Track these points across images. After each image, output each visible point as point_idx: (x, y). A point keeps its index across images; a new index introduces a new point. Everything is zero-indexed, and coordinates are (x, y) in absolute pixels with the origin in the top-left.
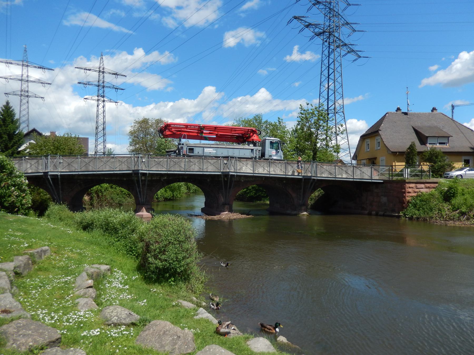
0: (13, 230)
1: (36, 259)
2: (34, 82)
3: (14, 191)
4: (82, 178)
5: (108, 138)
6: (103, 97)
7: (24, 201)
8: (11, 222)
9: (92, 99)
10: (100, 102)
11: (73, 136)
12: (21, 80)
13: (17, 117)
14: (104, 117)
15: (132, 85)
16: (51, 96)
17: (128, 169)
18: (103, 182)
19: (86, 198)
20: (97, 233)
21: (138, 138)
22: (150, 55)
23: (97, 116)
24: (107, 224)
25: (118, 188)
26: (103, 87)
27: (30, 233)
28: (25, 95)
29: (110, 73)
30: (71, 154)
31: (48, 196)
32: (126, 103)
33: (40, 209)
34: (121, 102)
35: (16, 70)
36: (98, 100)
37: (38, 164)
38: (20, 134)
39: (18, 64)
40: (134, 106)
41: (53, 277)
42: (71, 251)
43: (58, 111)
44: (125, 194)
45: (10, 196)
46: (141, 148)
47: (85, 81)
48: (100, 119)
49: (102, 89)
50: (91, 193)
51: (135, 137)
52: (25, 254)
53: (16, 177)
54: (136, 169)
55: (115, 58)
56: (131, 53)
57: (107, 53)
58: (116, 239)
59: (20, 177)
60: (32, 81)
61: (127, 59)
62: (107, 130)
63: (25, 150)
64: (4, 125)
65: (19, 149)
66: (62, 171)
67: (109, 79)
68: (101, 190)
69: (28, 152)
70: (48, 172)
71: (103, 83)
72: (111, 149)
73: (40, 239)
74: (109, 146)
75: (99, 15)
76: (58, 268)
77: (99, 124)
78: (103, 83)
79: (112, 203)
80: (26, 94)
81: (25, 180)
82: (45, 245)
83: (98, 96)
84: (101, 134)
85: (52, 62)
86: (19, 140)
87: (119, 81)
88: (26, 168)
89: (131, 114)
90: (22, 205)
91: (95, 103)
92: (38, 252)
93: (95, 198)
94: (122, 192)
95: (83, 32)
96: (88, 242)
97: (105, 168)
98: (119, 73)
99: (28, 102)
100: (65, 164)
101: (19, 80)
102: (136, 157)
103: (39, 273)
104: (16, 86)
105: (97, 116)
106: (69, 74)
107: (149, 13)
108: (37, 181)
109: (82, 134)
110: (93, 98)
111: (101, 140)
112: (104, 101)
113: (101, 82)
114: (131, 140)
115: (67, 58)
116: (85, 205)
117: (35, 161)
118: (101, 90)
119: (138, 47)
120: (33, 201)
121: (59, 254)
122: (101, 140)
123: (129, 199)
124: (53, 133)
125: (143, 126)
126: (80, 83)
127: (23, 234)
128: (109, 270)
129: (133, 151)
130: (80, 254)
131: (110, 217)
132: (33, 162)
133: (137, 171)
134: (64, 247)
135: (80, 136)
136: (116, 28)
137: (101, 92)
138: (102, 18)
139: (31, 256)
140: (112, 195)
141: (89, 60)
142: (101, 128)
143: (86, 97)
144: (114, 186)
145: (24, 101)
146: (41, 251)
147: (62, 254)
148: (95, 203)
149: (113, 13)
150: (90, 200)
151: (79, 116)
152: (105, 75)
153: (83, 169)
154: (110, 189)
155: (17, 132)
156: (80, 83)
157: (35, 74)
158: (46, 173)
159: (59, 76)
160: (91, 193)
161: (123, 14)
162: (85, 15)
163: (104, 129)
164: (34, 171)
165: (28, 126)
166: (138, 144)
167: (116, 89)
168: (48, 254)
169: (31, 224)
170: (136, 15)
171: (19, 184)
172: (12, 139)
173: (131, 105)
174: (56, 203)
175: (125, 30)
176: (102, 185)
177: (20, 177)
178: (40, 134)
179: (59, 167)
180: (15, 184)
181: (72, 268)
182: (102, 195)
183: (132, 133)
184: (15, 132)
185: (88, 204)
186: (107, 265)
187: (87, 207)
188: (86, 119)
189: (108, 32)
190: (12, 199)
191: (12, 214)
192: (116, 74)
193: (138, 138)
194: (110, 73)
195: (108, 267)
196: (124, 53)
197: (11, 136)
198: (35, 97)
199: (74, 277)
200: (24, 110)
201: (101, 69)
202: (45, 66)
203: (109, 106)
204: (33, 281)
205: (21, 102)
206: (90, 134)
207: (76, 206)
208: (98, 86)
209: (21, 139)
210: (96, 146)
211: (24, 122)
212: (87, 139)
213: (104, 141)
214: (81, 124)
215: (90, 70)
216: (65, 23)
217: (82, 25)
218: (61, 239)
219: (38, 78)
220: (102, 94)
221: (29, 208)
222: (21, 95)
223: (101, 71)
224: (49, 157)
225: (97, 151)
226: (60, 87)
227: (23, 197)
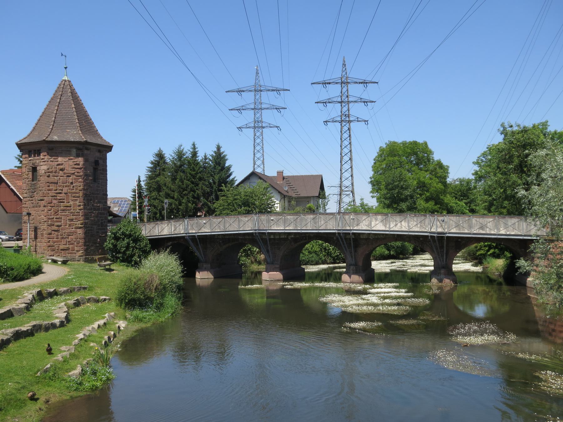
49: (347, 106)
167: (364, 102)
220: (347, 113)
222: (255, 127)
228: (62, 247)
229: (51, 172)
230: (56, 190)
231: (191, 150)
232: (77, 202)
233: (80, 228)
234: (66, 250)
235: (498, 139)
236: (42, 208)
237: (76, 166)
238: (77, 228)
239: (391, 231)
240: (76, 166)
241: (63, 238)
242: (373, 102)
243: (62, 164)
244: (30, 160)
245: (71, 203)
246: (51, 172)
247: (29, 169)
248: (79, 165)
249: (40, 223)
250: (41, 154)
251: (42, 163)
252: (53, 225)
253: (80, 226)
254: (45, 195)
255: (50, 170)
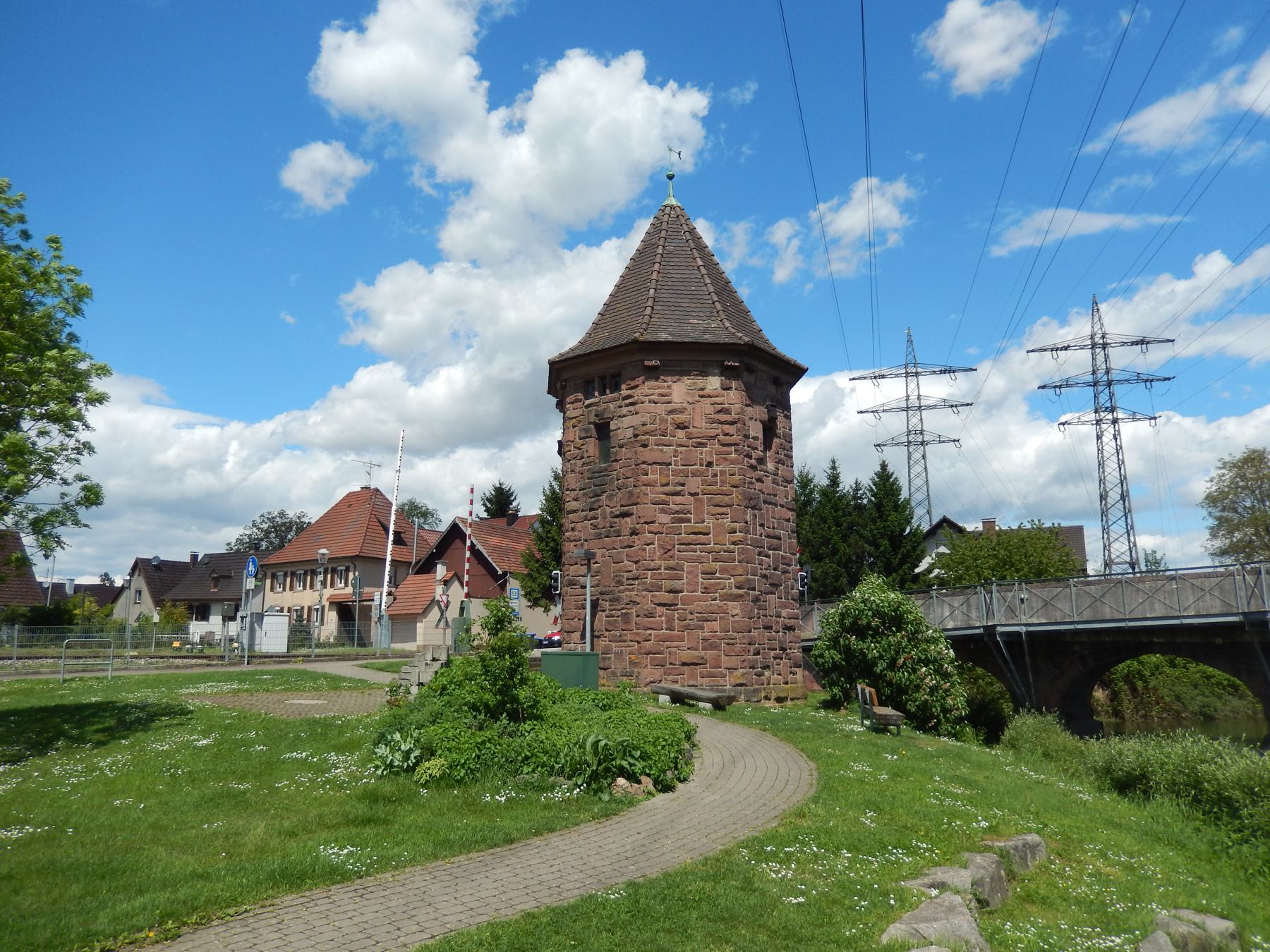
0: (943, 777)
1: (1015, 868)
2: (934, 407)
3: (926, 676)
4: (1085, 639)
5: (1138, 519)
6: (1112, 410)
7: (950, 701)
8: (933, 756)
9: (1080, 422)
10: (1104, 426)
11: (1048, 524)
12: (907, 409)
13: (904, 494)
14: (1121, 464)
15: (1198, 362)
16: (976, 434)
17: (1224, 610)
18: (1150, 650)
19: (1099, 694)
20: (1165, 809)
21: (1235, 511)
22: (1247, 262)
23: (1101, 465)
24: (1197, 784)
25: (1193, 667)
26: (1109, 384)
27: (984, 790)
28: (916, 440)
29: (1124, 344)
30: (1039, 575)
31: (998, 686)
32: (1184, 415)
33: (988, 724)
34: (1166, 413)
35: (894, 389)
36: (1098, 422)
37: (969, 606)
38: (914, 533)
39: (897, 376)
40: (1213, 417)
41: (1071, 927)
42: (1103, 854)
43: (996, 465)
44: (1218, 684)
45: (918, 688)
46: (1251, 541)
47: (1057, 379)
48: (1108, 470)
49: (1107, 391)
50: (1111, 681)
51: (1223, 510)
52: (988, 849)
53: (928, 641)
54: (1253, 609)
55: (1137, 298)
56: (1185, 272)
57: (1112, 294)
58: (1234, 836)
59: (935, 641)
60: (928, 407)
61: (1173, 291)
62: (1135, 499)
63: (929, 570)
64: (880, 517)
65: (917, 571)
66: (1030, 621)
67: (1122, 359)
68: (1139, 672)
69: (936, 577)
70: (995, 626)
71: (1107, 373)
72: (1155, 552)
73: (1013, 811)
74: (1145, 542)
75: (1081, 205)
76: (1078, 902)
77: (1109, 486)
78: (1107, 373)
79: (1178, 713)
80: (920, 438)
81: (947, 648)
82: (1030, 831)
83: (1096, 411)
84: (1116, 513)
85: (973, 351)
86: (914, 549)
87: (1155, 359)
88: (945, 616)
89: (1201, 443)
90: (945, 711)
91: (1091, 430)
92: (1016, 848)
93: (1126, 695)
94: (1209, 678)
95: (1042, 261)
96: (1146, 834)
97: (1152, 609)
98: (1150, 336)
99: (924, 457)
100: (1037, 604)
101: (902, 409)
102: (1251, 572)
103: (1033, 909)
104: (896, 424)
105: (1101, 465)
106: (1013, 371)
107: (1229, 150)
108: (975, 648)
109: (1062, 518)
110: (1083, 419)
111: (1118, 529)
112: (1115, 421)
113: (1101, 373)
114: (1211, 522)
115: (1005, 332)
116: (1098, 714)
117: (961, 598)
118: (1104, 391)
119: (1207, 251)
120: (970, 702)
121: (1069, 860)
122: (1118, 529)
123: (1235, 702)
124: (989, 524)
125: (1250, 472)
126: (1043, 387)
127: (968, 792)
128: (1233, 936)
129: (1223, 553)
130: (1129, 868)
131: (1202, 762)
132: (957, 601)
133: (1260, 617)
134: (1081, 841)
135: (1064, 524)
136: (1129, 222)
137: (1104, 398)
138: (1091, 209)
139: (1001, 856)
140: (1178, 688)
141: (1064, 322)
142: (1114, 495)
143: (1063, 419)
144: (1179, 660)
145: (917, 455)
146: (1024, 846)
147: (1079, 862)
148: (1127, 707)
149: (1121, 188)
150: (1112, 700)
151: (1051, 470)
152: (1110, 350)
153: (1087, 615)
154: (1168, 670)
155: (908, 530)
156: (1043, 387)
157: (935, 388)
158: (990, 630)
159: (991, 379)
160: (1111, 681)
161: (1149, 181)
162: (1044, 217)
163: (1124, 497)
164: (959, 624)
165: (929, 512)
166: (1238, 528)
167: (1146, 381)
168: (1041, 857)
169: (980, 766)
170: (1188, 169)
171: (935, 660)
172: (899, 547)
173: (1203, 417)
174: (1029, 711)
175: (1157, 220)
176: (1144, 658)
177: (935, 641)
178: (961, 530)
179: (1022, 611)
180: (927, 658)
181: (1117, 910)
182: (1146, 688)
183: (1211, 500)
184: (904, 530)
185: (1107, 712)
186: (1223, 917)
187: (1103, 719)
188: (1068, 475)
189: (1112, 235)
190: (923, 696)
191: (925, 732)
192: (1142, 342)
193: (1235, 511)
194: (1124, 344)
195: (1229, 925)
196: (1165, 277)
197: (897, 539)
198: (940, 442)
199: (1130, 942)
200: (918, 475)
201: (1098, 340)
202: (955, 364)
203: (1129, 430)
204: (1020, 930)
205: (909, 458)
206: (1086, 514)
207: (1081, 721)
208: (1095, 384)
209: (919, 544)
210: (1107, 547)
211: (919, 504)
212: (1080, 530)
213: (1130, 530)
214: (1056, 491)
215: (1066, 348)
216: (997, 251)
217: (1038, 244)
218: (1066, 816)
219: (943, 396)
220: (1108, 404)
221: (960, 720)
222: (909, 442)
223: (1099, 344)
224: (994, 587)
225: (1112, 561)
226: (994, 406)
227: (947, 691)
228: (686, 655)
229: (651, 433)
230: (667, 485)
231: (829, 471)
232: (727, 521)
233: (737, 598)
234: (696, 664)
235: (1015, 527)
236: (625, 538)
237: (722, 417)
238: (725, 598)
239: (1184, 617)
240: (722, 417)
241: (687, 627)
242: (1169, 379)
243: (682, 411)
244: (588, 406)
245: (709, 522)
246: (651, 433)
247: (587, 430)
248: (727, 411)
249: (620, 583)
250: (623, 387)
251: (625, 410)
252: (659, 589)
253: (735, 591)
254: (633, 500)
255: (650, 427)
